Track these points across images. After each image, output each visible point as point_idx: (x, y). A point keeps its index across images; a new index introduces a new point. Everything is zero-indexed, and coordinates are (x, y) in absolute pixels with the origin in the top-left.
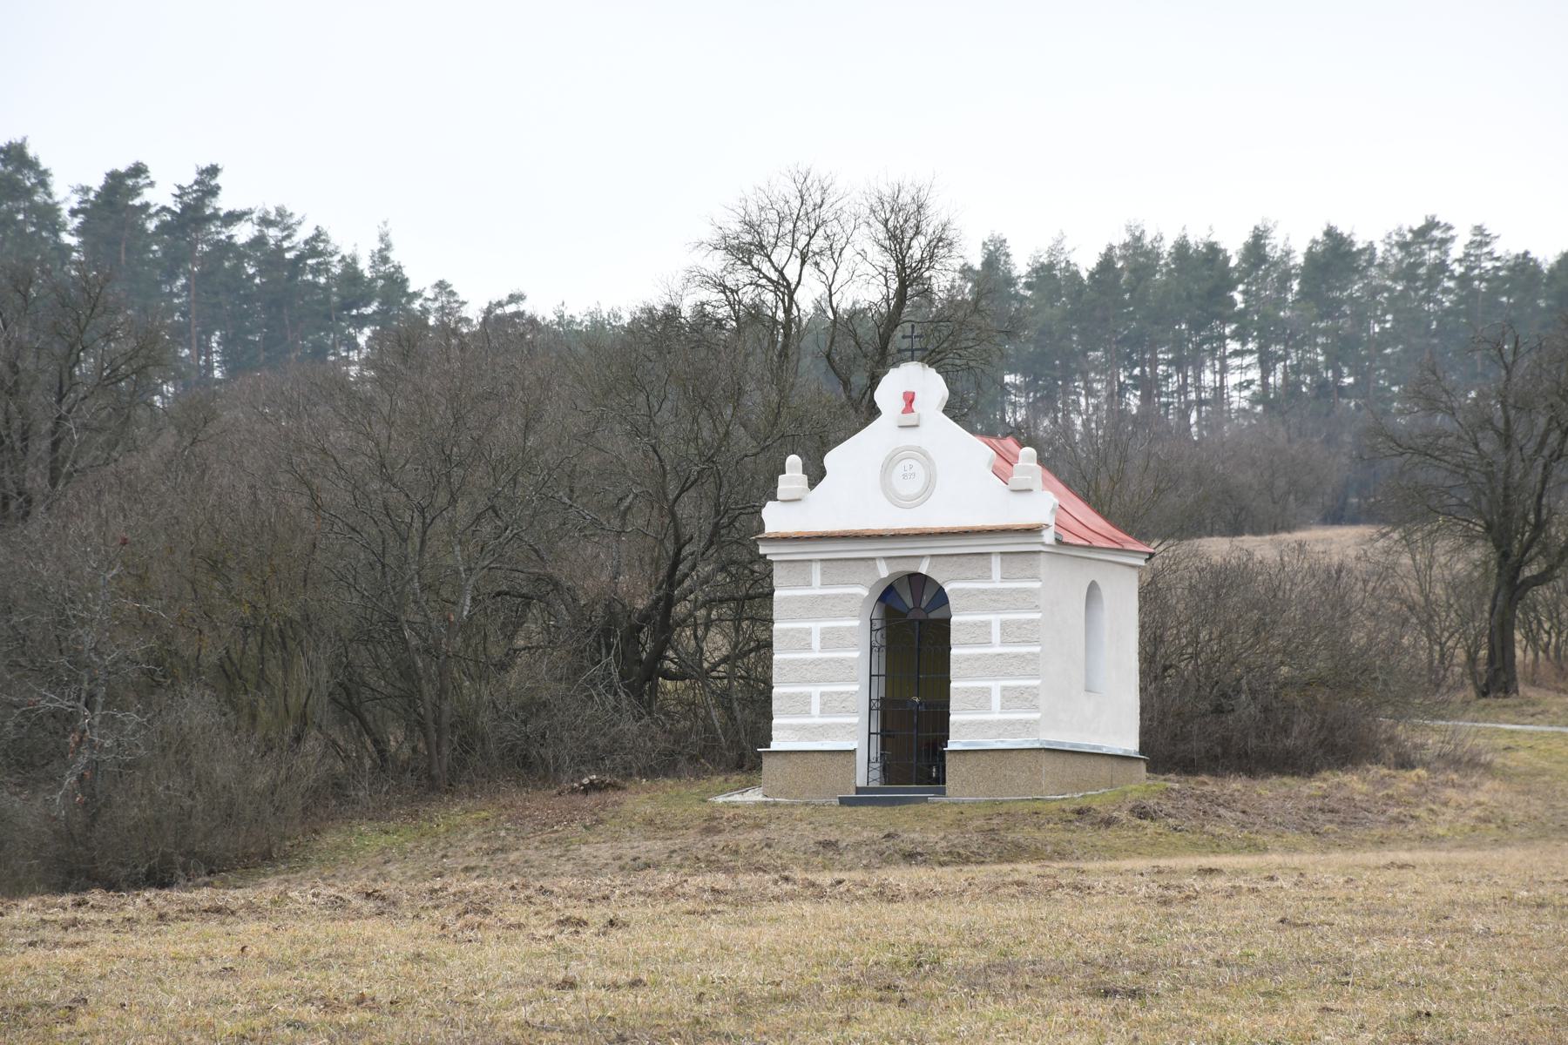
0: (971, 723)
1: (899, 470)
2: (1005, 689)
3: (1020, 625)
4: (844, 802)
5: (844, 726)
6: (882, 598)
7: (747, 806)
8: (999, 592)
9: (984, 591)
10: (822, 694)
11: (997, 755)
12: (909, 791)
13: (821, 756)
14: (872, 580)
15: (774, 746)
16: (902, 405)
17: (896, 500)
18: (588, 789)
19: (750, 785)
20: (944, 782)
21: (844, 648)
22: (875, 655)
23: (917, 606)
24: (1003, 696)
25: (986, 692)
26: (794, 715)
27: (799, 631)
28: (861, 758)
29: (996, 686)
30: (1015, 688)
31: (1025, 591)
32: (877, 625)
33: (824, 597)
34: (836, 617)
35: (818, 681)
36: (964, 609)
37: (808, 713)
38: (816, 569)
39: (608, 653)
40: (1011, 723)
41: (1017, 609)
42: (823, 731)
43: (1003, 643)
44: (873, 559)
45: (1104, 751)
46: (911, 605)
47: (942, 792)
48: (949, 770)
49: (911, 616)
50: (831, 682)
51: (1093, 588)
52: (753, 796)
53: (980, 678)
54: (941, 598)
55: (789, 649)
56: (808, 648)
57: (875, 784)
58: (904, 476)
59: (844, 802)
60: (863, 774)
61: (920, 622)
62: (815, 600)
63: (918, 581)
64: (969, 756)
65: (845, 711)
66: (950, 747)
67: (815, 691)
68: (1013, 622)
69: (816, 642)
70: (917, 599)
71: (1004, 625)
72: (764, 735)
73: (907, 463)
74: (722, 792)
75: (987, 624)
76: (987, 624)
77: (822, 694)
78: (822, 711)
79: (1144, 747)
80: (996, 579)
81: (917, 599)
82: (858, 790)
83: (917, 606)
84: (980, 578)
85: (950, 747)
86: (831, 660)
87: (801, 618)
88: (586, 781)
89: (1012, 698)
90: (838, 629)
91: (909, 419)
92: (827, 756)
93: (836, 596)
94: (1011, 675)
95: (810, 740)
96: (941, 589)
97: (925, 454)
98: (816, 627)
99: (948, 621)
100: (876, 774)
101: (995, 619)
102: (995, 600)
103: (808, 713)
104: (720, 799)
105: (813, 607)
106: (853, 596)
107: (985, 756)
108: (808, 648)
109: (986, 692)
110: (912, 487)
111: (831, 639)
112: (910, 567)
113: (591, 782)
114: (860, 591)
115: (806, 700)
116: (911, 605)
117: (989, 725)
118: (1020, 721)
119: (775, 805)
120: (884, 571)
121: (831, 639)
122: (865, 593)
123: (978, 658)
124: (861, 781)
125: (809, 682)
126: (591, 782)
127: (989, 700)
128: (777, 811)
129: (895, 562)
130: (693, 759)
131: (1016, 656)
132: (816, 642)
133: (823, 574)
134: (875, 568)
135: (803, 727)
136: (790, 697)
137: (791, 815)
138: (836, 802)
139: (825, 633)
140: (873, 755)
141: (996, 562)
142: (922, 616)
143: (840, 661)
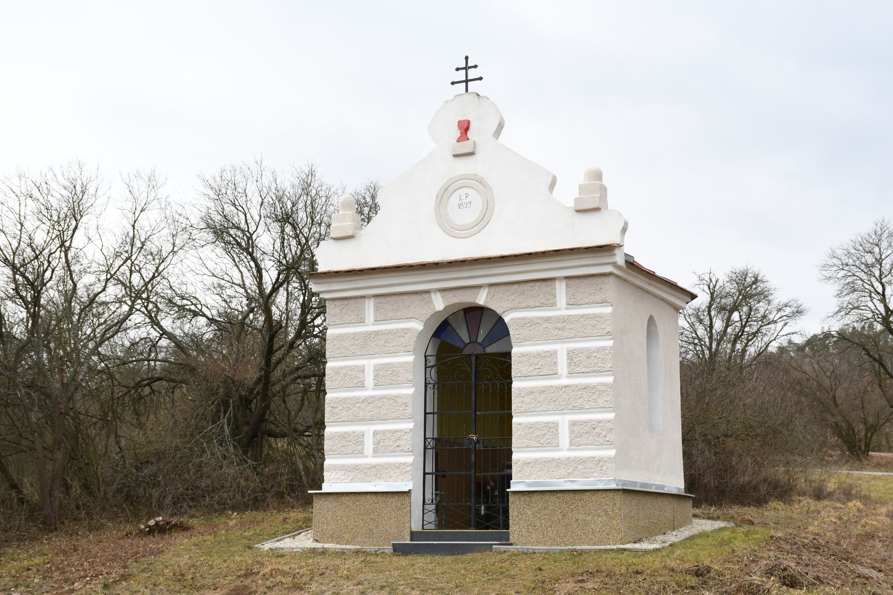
0: (536, 461)
1: (454, 200)
2: (573, 424)
3: (589, 354)
4: (400, 550)
5: (397, 466)
6: (437, 334)
7: (294, 555)
8: (564, 320)
9: (548, 320)
10: (375, 433)
11: (567, 497)
12: (469, 537)
13: (374, 498)
14: (427, 313)
15: (326, 488)
16: (457, 133)
17: (453, 231)
18: (151, 531)
19: (306, 524)
20: (507, 526)
21: (399, 384)
22: (430, 392)
23: (473, 341)
24: (572, 432)
25: (553, 428)
26: (346, 455)
27: (352, 368)
28: (416, 499)
29: (564, 421)
30: (585, 423)
31: (595, 316)
32: (432, 361)
33: (377, 333)
34: (389, 354)
35: (371, 420)
36: (525, 340)
37: (361, 453)
38: (370, 306)
39: (224, 418)
40: (582, 461)
41: (586, 337)
42: (376, 471)
43: (571, 374)
44: (427, 292)
45: (666, 491)
46: (467, 340)
47: (505, 539)
48: (513, 513)
49: (466, 351)
50: (385, 420)
51: (651, 321)
52: (304, 541)
53: (545, 412)
54: (500, 329)
55: (339, 388)
56: (361, 386)
57: (431, 527)
58: (460, 206)
59: (400, 550)
60: (418, 516)
61: (477, 357)
62: (368, 336)
63: (474, 314)
64: (535, 498)
65: (398, 450)
66: (514, 488)
67: (368, 430)
68: (581, 351)
69: (369, 381)
70: (473, 331)
71: (572, 355)
72: (318, 481)
73: (462, 192)
74: (273, 535)
75: (553, 354)
76: (553, 354)
77: (375, 433)
78: (375, 451)
79: (691, 482)
80: (563, 304)
81: (473, 331)
82: (414, 535)
83: (473, 341)
84: (542, 306)
85: (514, 488)
86: (384, 397)
87: (354, 356)
88: (152, 522)
89: (582, 434)
90: (392, 365)
91: (465, 147)
92: (380, 498)
93: (390, 332)
94: (580, 409)
95: (363, 481)
96: (500, 320)
97: (481, 181)
98: (370, 364)
99: (508, 355)
100: (431, 517)
101: (562, 349)
102: (561, 329)
103: (361, 453)
104: (267, 546)
105: (366, 344)
106: (407, 331)
107: (553, 498)
108: (361, 386)
109: (553, 428)
110: (469, 216)
111: (384, 376)
112: (466, 299)
113: (157, 523)
114: (414, 325)
115: (359, 439)
116: (467, 340)
117: (558, 463)
118: (592, 459)
119: (324, 552)
120: (439, 304)
121: (384, 376)
122: (420, 327)
123: (543, 391)
124: (416, 526)
125: (362, 421)
126: (157, 523)
127: (556, 435)
128: (323, 562)
129: (451, 294)
130: (280, 496)
131: (585, 388)
132: (369, 381)
133: (377, 309)
134: (430, 301)
135: (355, 468)
136: (343, 436)
137: (336, 569)
138: (389, 549)
139: (378, 369)
140: (429, 496)
141: (561, 289)
142: (479, 350)
143: (394, 398)
